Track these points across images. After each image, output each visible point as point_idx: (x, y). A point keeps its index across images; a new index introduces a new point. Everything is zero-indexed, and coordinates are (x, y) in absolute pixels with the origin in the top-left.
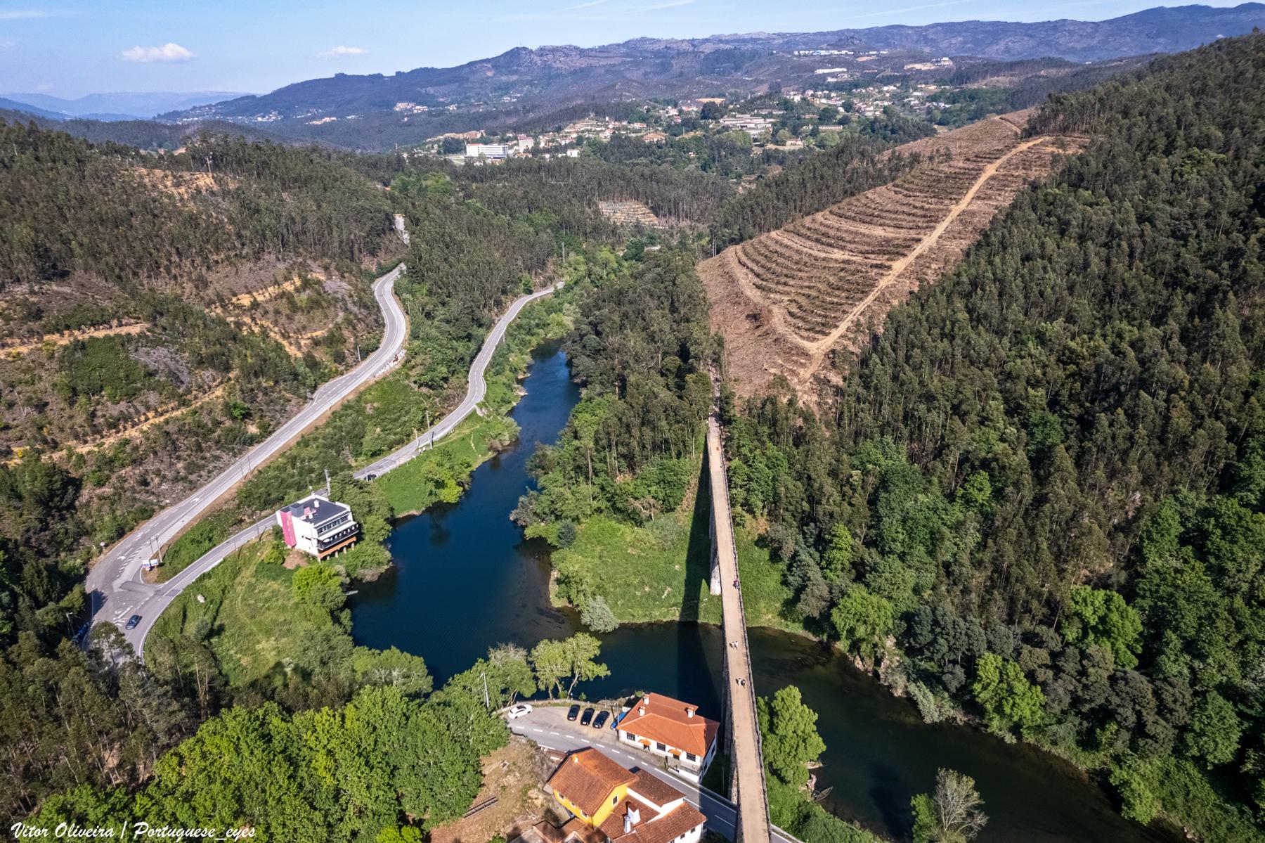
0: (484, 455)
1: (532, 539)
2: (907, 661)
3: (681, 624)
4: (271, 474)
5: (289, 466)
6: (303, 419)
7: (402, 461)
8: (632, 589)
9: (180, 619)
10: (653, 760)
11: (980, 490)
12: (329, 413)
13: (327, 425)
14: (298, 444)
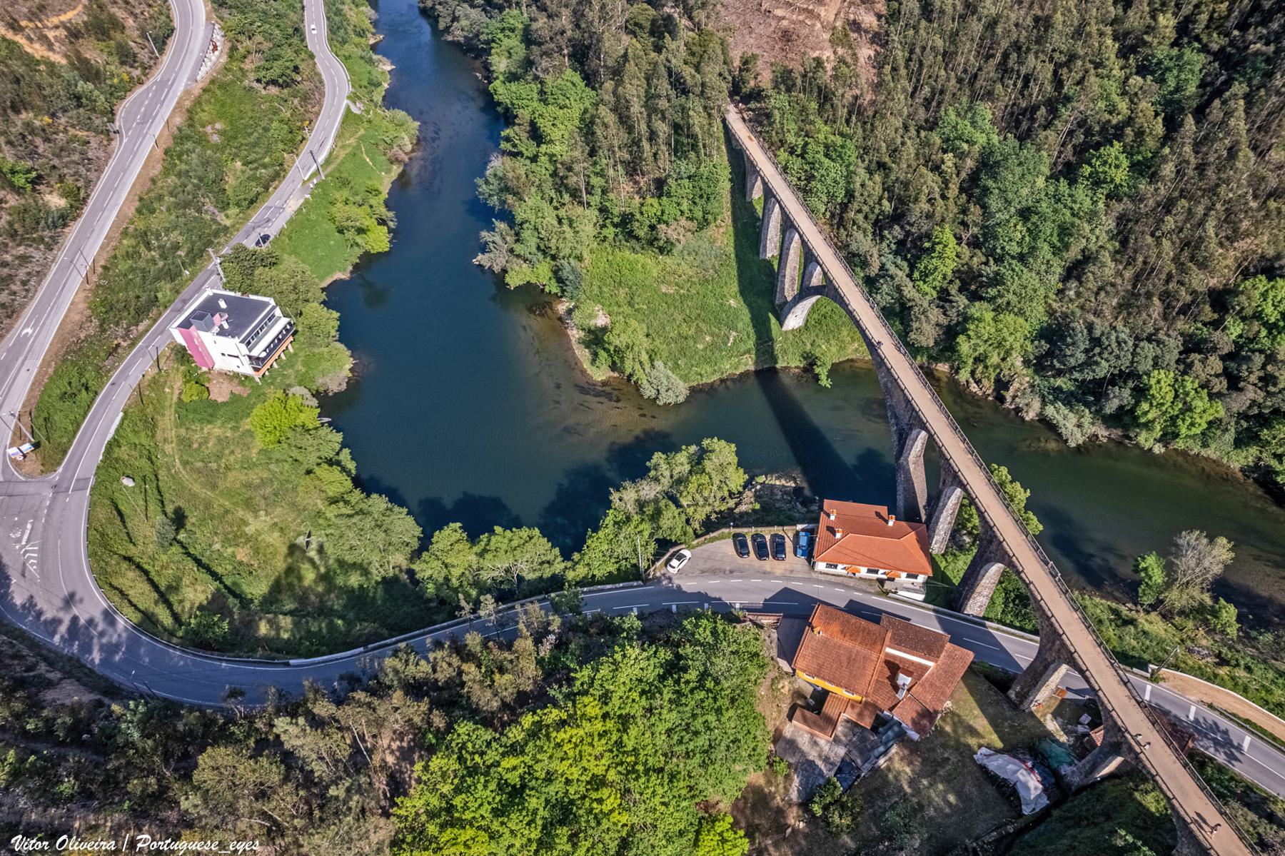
0: (388, 171)
1: (518, 288)
2: (1038, 380)
3: (758, 373)
4: (123, 266)
5: (142, 249)
6: (123, 169)
7: (293, 205)
8: (691, 343)
9: (118, 521)
10: (864, 586)
11: (1117, 167)
12: (159, 152)
13: (166, 172)
14: (139, 211)
